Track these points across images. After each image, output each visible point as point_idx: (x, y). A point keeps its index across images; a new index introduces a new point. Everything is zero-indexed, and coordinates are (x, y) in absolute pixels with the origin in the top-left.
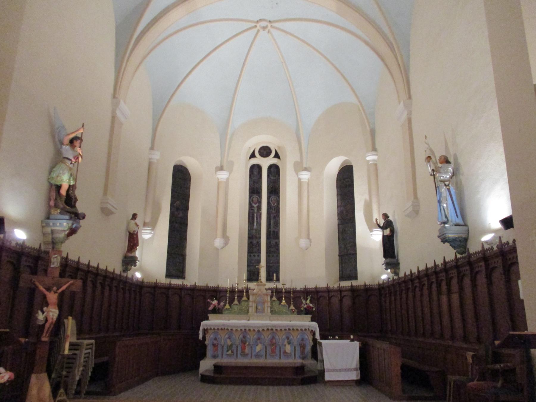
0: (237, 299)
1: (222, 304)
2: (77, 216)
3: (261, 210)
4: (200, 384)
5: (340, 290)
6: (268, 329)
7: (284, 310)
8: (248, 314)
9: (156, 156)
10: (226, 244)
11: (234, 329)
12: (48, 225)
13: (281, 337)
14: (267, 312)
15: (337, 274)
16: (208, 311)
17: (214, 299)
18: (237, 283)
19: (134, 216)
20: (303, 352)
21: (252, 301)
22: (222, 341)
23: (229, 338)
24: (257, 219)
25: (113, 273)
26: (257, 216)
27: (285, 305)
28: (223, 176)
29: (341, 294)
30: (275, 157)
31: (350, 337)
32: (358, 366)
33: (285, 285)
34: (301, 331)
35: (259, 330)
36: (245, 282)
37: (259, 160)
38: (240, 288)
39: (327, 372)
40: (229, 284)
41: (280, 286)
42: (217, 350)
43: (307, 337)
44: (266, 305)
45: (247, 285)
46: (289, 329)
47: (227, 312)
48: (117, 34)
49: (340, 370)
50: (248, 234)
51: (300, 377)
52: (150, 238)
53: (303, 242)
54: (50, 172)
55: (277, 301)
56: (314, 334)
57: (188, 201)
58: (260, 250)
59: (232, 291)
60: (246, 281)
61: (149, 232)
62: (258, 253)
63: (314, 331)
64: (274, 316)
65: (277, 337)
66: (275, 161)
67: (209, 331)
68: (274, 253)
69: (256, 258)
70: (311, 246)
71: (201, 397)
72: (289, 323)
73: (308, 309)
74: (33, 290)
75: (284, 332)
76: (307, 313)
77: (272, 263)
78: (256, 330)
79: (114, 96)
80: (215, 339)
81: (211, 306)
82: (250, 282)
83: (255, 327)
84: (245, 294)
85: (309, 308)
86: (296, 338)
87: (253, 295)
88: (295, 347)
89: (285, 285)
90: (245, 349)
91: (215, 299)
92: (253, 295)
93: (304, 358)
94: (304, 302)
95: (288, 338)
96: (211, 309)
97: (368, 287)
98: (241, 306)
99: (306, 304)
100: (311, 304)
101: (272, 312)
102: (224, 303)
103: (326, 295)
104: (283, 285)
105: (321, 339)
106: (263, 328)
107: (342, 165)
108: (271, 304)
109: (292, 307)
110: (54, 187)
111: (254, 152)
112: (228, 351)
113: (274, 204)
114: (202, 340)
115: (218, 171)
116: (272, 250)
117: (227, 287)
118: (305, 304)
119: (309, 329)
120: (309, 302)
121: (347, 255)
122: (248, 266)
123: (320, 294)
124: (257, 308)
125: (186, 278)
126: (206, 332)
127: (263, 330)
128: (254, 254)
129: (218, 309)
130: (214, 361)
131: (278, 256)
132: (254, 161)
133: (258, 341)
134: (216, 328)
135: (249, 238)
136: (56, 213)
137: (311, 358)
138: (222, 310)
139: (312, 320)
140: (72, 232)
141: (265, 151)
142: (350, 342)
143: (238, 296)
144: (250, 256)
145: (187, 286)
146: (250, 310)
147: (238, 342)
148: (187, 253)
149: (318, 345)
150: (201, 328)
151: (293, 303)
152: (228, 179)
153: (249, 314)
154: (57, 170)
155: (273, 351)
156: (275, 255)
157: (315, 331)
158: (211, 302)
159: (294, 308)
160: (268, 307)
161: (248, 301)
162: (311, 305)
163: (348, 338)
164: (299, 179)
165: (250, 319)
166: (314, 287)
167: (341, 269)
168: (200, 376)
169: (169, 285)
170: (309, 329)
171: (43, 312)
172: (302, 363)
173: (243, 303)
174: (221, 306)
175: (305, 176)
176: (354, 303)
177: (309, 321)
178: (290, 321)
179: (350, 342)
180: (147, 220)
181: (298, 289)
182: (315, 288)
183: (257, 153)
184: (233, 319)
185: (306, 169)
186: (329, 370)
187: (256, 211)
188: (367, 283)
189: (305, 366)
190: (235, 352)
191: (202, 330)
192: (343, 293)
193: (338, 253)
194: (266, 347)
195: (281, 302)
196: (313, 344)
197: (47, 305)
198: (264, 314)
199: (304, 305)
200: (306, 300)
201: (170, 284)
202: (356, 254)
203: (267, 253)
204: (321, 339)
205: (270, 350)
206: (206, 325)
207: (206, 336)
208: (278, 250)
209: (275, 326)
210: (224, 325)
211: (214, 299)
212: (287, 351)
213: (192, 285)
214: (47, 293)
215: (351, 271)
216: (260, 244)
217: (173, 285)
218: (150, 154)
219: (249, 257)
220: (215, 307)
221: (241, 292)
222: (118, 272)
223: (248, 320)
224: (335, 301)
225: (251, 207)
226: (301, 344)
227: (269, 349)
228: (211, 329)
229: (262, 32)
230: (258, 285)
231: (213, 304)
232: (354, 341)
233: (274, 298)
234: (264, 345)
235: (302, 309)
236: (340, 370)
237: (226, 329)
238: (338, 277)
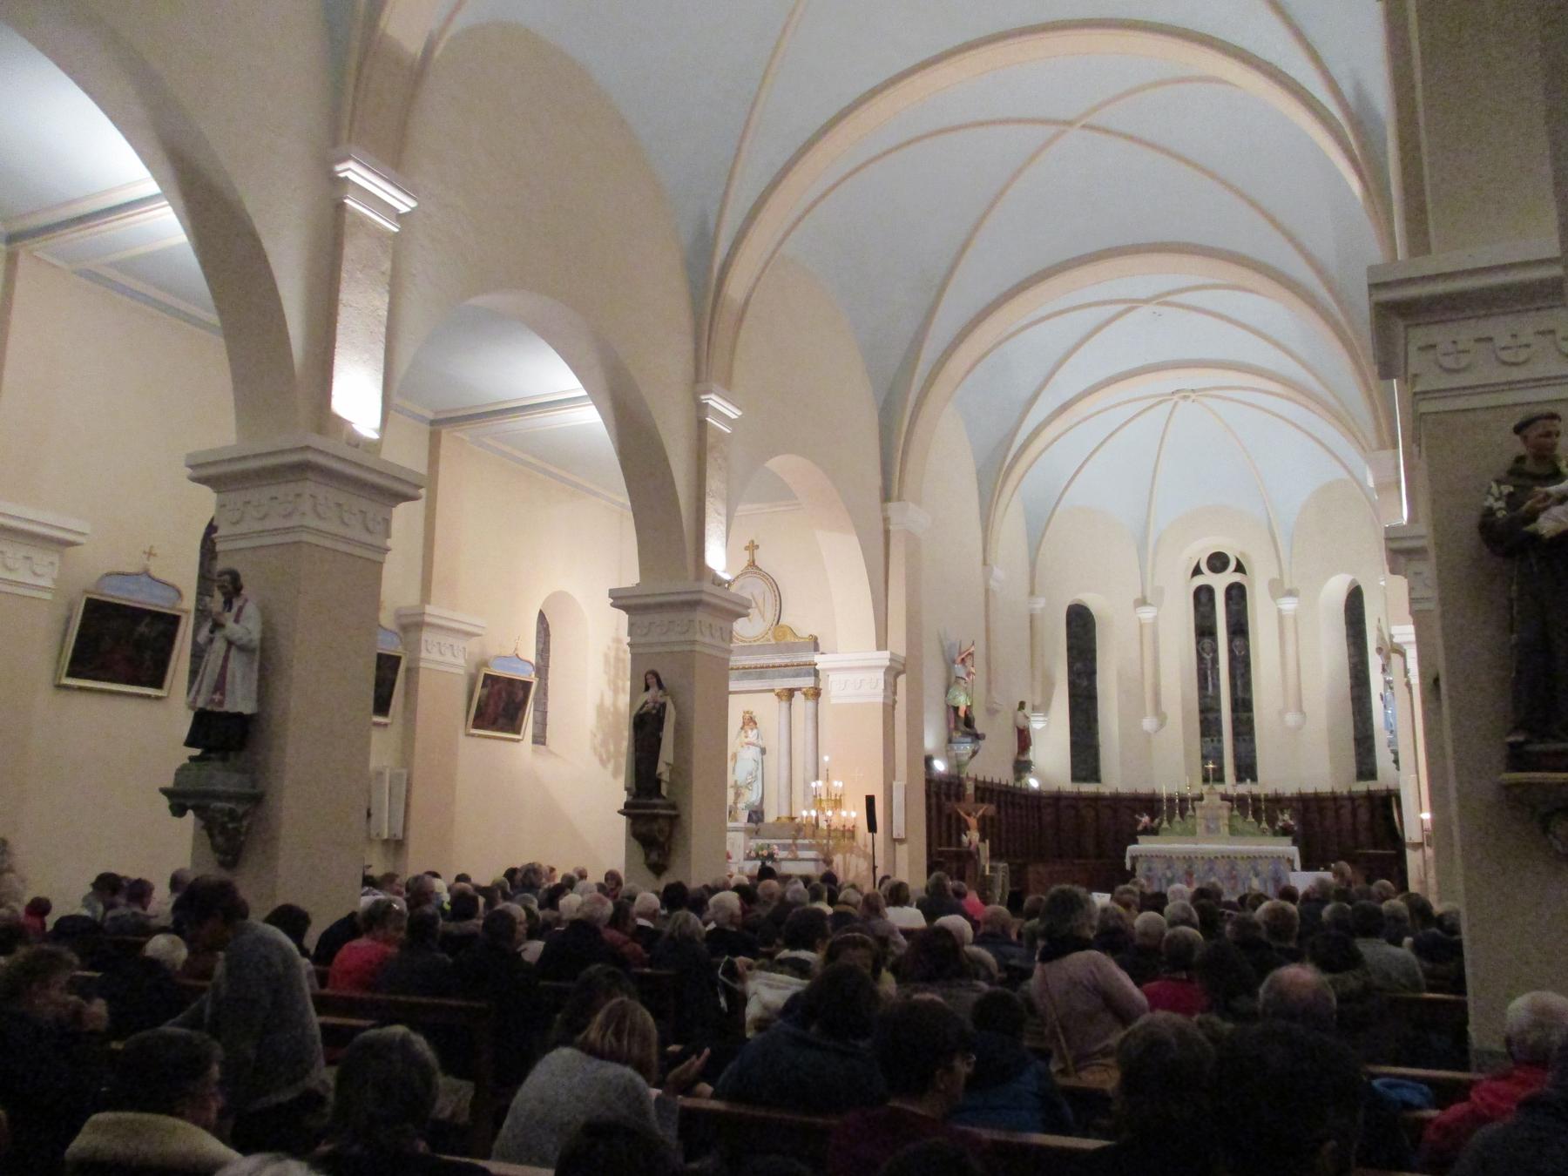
1: (1157, 821)
2: (977, 737)
3: (1218, 664)
5: (1351, 797)
9: (1040, 604)
10: (1162, 724)
12: (952, 749)
13: (1242, 867)
15: (1353, 770)
19: (1022, 705)
24: (1213, 678)
25: (1007, 786)
26: (1212, 673)
28: (1147, 614)
30: (1236, 571)
37: (1208, 578)
41: (1256, 789)
44: (1221, 823)
48: (980, 483)
50: (1200, 704)
52: (1043, 728)
53: (1291, 718)
54: (947, 693)
57: (1093, 659)
59: (1171, 800)
61: (1041, 719)
66: (1237, 578)
67: (1140, 859)
72: (1193, 846)
74: (959, 818)
79: (985, 563)
80: (1150, 869)
86: (1265, 868)
94: (1280, 817)
107: (1349, 587)
109: (1264, 825)
110: (952, 710)
111: (1198, 563)
113: (1240, 652)
115: (1139, 606)
127: (1196, 857)
131: (1252, 741)
132: (1200, 581)
133: (1211, 873)
135: (1202, 711)
136: (957, 735)
140: (975, 753)
141: (1218, 562)
146: (1198, 829)
152: (1156, 618)
154: (954, 692)
156: (1247, 738)
162: (1292, 823)
164: (1280, 611)
170: (1283, 857)
171: (966, 835)
175: (1288, 605)
180: (1037, 702)
183: (1204, 567)
185: (1291, 593)
187: (1209, 665)
195: (1246, 817)
197: (969, 829)
214: (967, 817)
218: (1029, 603)
222: (1011, 783)
224: (1346, 813)
225: (1200, 659)
228: (1141, 856)
229: (1181, 403)
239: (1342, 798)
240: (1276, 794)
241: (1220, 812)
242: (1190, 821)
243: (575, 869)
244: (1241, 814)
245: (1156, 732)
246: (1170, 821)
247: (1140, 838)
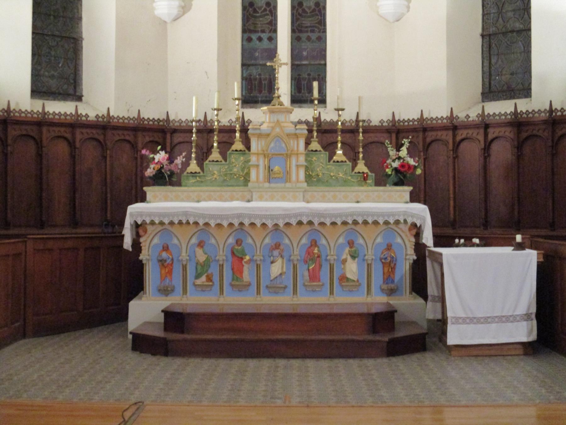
0: (218, 147)
1: (179, 160)
4: (134, 358)
6: (300, 223)
7: (341, 175)
8: (246, 185)
11: (213, 223)
14: (298, 181)
16: (143, 177)
17: (159, 148)
18: (215, 107)
20: (388, 277)
21: (256, 152)
22: (184, 254)
23: (201, 244)
27: (342, 162)
29: (486, 135)
31: (515, 238)
32: (534, 310)
33: (343, 110)
34: (385, 227)
35: (276, 225)
36: (238, 105)
38: (225, 122)
39: (453, 323)
40: (197, 111)
42: (170, 272)
43: (399, 240)
45: (243, 113)
46: (355, 223)
47: (192, 180)
49: (486, 320)
51: (386, 338)
55: (323, 152)
56: (417, 231)
58: (276, 25)
60: (240, 101)
62: (270, 32)
63: (418, 225)
64: (314, 188)
65: (324, 242)
67: (150, 228)
68: (312, 31)
69: (265, 44)
70: (408, 11)
71: (135, 388)
72: (303, 205)
73: (402, 170)
75: (382, 227)
76: (399, 183)
77: (306, 58)
78: (270, 224)
80: (166, 248)
81: (152, 166)
82: (251, 108)
83: (266, 217)
84: (238, 135)
85: (407, 167)
87: (260, 136)
88: (369, 266)
89: (343, 110)
90: (241, 272)
91: (162, 149)
92: (260, 136)
93: (391, 292)
94: (392, 152)
95: (351, 244)
96: (151, 175)
97: (559, 114)
98: (230, 163)
99: (399, 158)
100: (411, 157)
101: (309, 178)
102: (183, 158)
103: (448, 136)
104: (338, 110)
105: (436, 245)
106: (287, 220)
108: (306, 160)
109: (361, 167)
112: (198, 276)
114: (131, 250)
116: (307, 22)
117: (189, 119)
118: (394, 157)
119: (405, 221)
120: (406, 152)
121: (504, 34)
122: (244, 65)
123: (431, 136)
124: (270, 170)
125: (83, 98)
126: (141, 232)
127: (253, 224)
128: (260, 34)
129: (169, 173)
130: (165, 302)
131: (322, 39)
133: (276, 253)
134: (166, 221)
137: (411, 293)
138: (179, 175)
139: (414, 198)
142: (514, 250)
143: (219, 143)
144: (250, 40)
145: (89, 119)
147: (222, 255)
148: (85, 35)
149: (428, 259)
150: (128, 222)
151: (363, 157)
153: (250, 184)
155: (314, 277)
156: (314, 36)
157: (420, 226)
158: (152, 156)
159: (366, 170)
160: (298, 166)
161: (247, 151)
162: (412, 162)
163: (508, 241)
165: (252, 197)
166: (416, 116)
167: (487, 69)
168: (130, 337)
169: (105, 120)
172: (388, 304)
173: (233, 158)
174: (177, 165)
176: (519, 157)
177: (407, 203)
178: (358, 202)
179: (514, 250)
181: (375, 122)
182: (418, 119)
184: (210, 199)
186: (457, 320)
188: (557, 105)
189: (396, 311)
190: (216, 278)
191: (131, 225)
192: (491, 131)
193: (480, 30)
194: (295, 267)
195: (332, 154)
196: (415, 258)
198: (288, 185)
199: (394, 161)
200: (398, 147)
201: (44, 113)
202: (530, 30)
203: (293, 31)
204: (436, 245)
205: (306, 273)
206: (141, 214)
207: (142, 240)
208: (322, 23)
209: (320, 214)
210: (186, 213)
211: (159, 148)
212: (349, 275)
213: (100, 115)
215: (512, 74)
216: (275, 7)
217: (51, 116)
219: (245, 43)
220: (162, 168)
221: (228, 131)
223: (249, 201)
226: (386, 258)
227: (303, 273)
228: (152, 223)
230: (272, 112)
231: (156, 161)
232: (525, 250)
233: (315, 145)
234: (289, 260)
235: (389, 171)
236: (486, 320)
237: (191, 223)
238: (480, 90)
239: (468, 126)
240: (551, 111)
241: (293, 143)
242: (236, 161)
243: (125, 234)
244: (325, 148)
245: (176, 19)
246: (201, 163)
247: (150, 191)
